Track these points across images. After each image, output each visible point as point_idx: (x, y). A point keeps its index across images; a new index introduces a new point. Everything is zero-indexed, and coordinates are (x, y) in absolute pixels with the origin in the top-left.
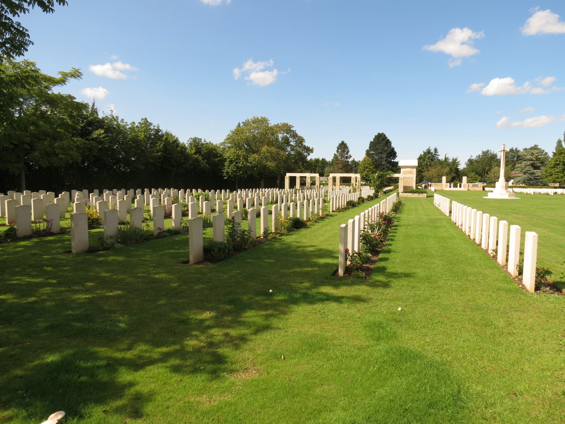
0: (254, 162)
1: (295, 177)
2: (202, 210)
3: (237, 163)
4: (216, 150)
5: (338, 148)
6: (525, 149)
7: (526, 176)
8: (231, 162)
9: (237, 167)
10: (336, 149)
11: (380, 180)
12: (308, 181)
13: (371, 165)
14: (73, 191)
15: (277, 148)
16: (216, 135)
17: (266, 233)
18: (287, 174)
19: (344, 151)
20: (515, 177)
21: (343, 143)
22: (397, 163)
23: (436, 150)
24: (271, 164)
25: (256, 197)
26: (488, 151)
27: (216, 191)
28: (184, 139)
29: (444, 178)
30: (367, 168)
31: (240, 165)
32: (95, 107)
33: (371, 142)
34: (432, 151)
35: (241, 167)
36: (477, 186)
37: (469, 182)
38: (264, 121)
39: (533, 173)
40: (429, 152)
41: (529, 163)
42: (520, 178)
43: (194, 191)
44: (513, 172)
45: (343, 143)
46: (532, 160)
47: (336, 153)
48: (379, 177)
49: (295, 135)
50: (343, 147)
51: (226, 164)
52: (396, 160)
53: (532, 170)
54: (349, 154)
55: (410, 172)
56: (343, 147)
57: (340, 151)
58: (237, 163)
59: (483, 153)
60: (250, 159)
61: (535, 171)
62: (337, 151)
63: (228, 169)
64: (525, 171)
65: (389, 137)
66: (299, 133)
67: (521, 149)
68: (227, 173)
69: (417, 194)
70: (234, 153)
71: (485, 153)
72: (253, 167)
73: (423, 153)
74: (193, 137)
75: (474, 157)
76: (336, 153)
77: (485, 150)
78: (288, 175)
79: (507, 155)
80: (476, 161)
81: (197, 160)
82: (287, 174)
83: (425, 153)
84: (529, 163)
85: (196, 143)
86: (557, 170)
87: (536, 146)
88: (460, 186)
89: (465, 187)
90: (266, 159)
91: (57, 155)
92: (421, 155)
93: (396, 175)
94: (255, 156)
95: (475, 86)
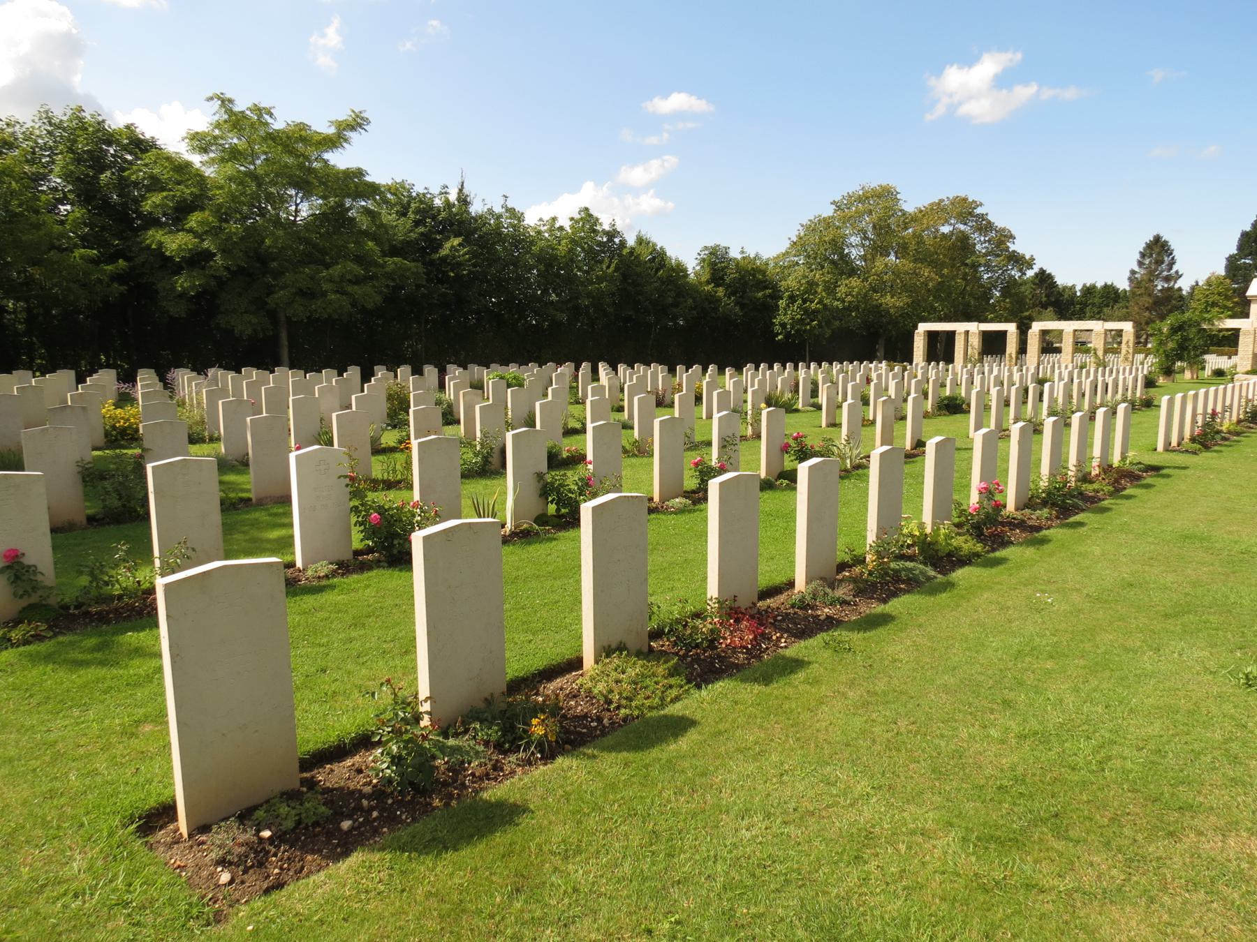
0: (849, 298)
1: (951, 335)
2: (631, 416)
3: (804, 301)
4: (764, 272)
5: (1143, 255)
8: (792, 299)
9: (806, 311)
10: (1138, 256)
11: (1178, 337)
12: (1097, 343)
13: (1227, 298)
14: (450, 367)
15: (915, 261)
16: (763, 233)
18: (920, 325)
19: (1159, 262)
21: (1157, 239)
24: (891, 302)
25: (965, 377)
27: (705, 370)
28: (685, 253)
30: (1214, 304)
31: (813, 306)
32: (464, 191)
33: (1245, 235)
35: (815, 312)
38: (886, 195)
43: (603, 369)
45: (1157, 239)
47: (1136, 268)
48: (1174, 330)
49: (985, 226)
50: (1158, 250)
51: (782, 303)
54: (1175, 268)
56: (1158, 250)
57: (1147, 261)
58: (804, 301)
60: (842, 290)
62: (1140, 264)
63: (785, 316)
66: (999, 220)
68: (783, 325)
70: (805, 277)
71: (1227, 259)
72: (848, 309)
74: (710, 244)
76: (1136, 268)
78: (923, 327)
79: (1042, 272)
81: (711, 299)
82: (920, 325)
85: (716, 262)
90: (901, 291)
91: (324, 294)
93: (1231, 323)
94: (855, 282)
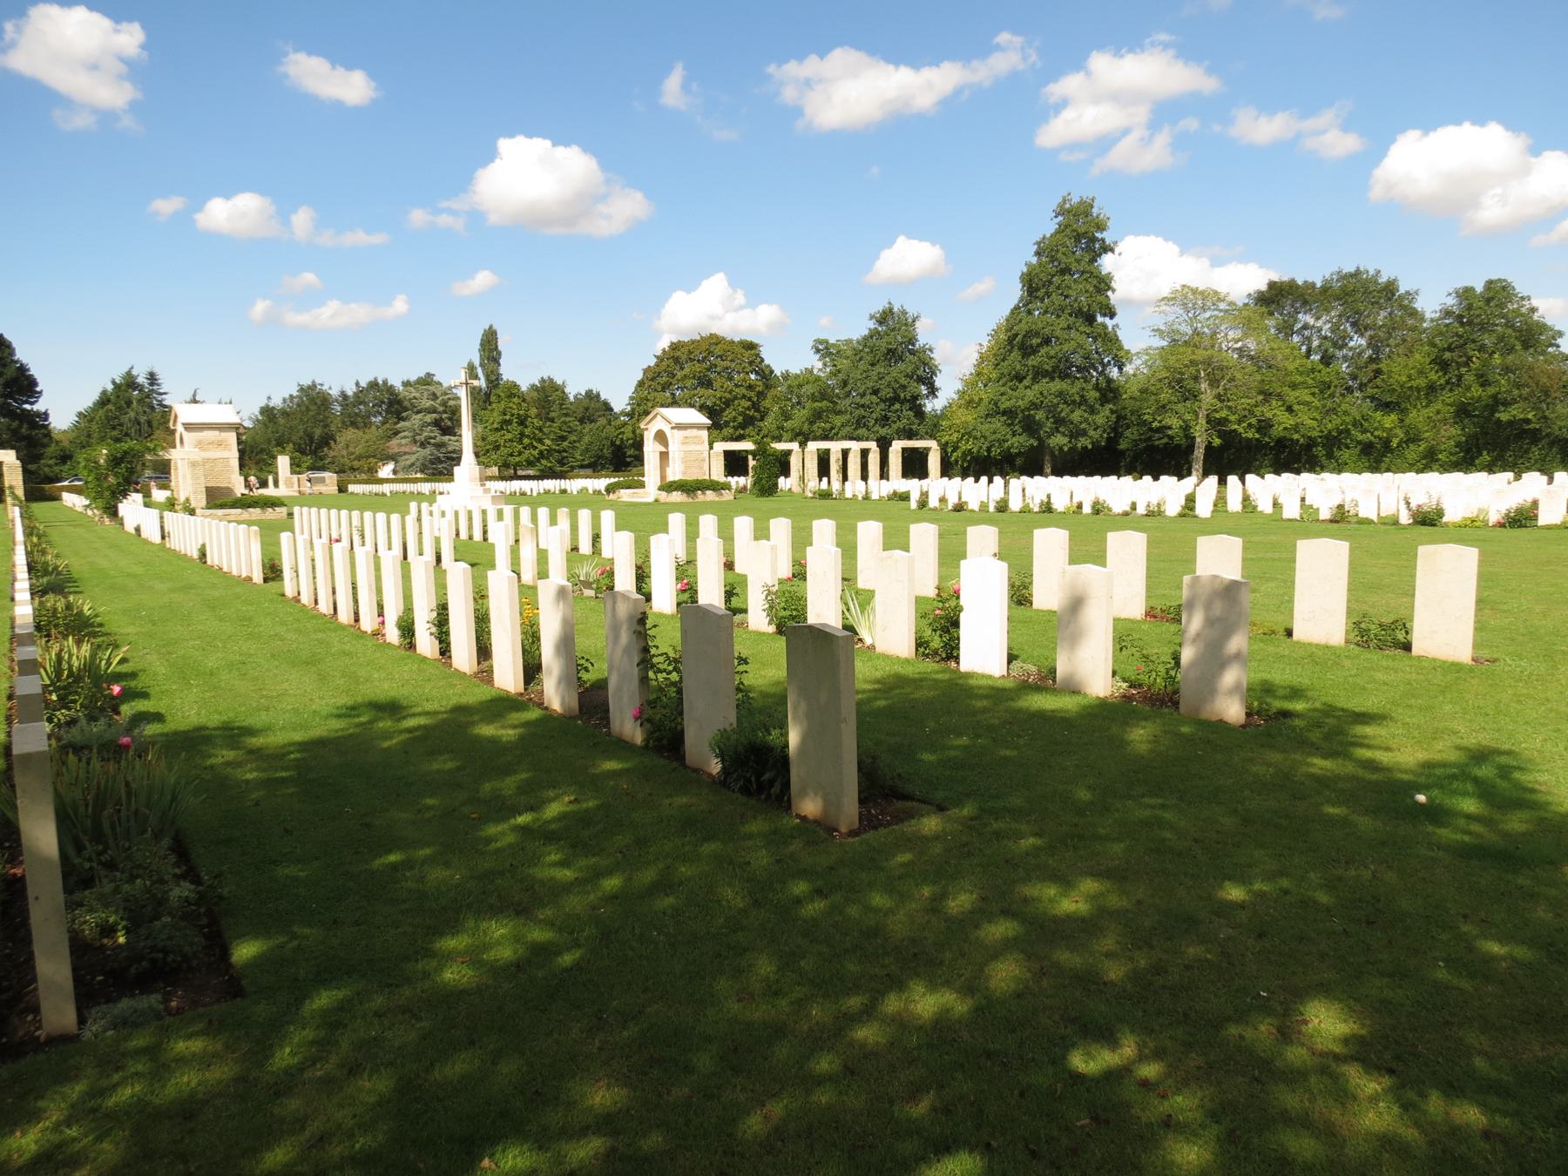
6: (406, 384)
7: (427, 451)
17: (489, 840)
20: (400, 454)
22: (46, 415)
23: (152, 378)
26: (314, 385)
29: (283, 462)
34: (141, 380)
36: (322, 480)
37: (296, 467)
39: (442, 445)
40: (130, 382)
41: (429, 418)
42: (413, 458)
44: (394, 442)
46: (435, 411)
52: (39, 406)
53: (440, 439)
55: (219, 444)
59: (302, 389)
61: (447, 438)
64: (422, 438)
65: (1494, 277)
67: (396, 382)
69: (258, 510)
73: (110, 387)
75: (277, 402)
77: (307, 382)
80: (284, 413)
83: (117, 386)
84: (429, 418)
86: (509, 436)
87: (428, 374)
88: (276, 484)
89: (289, 484)
92: (104, 392)
95: (166, 206)
